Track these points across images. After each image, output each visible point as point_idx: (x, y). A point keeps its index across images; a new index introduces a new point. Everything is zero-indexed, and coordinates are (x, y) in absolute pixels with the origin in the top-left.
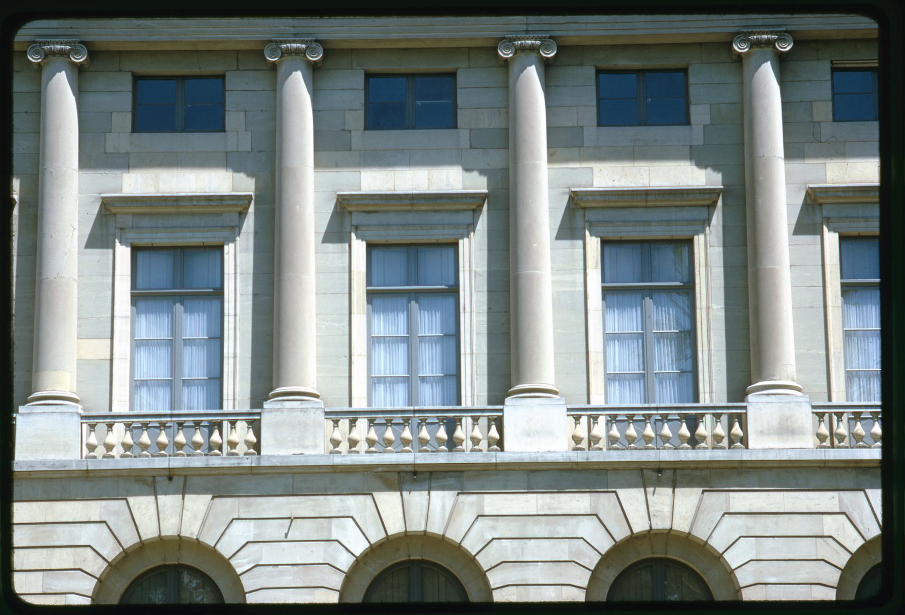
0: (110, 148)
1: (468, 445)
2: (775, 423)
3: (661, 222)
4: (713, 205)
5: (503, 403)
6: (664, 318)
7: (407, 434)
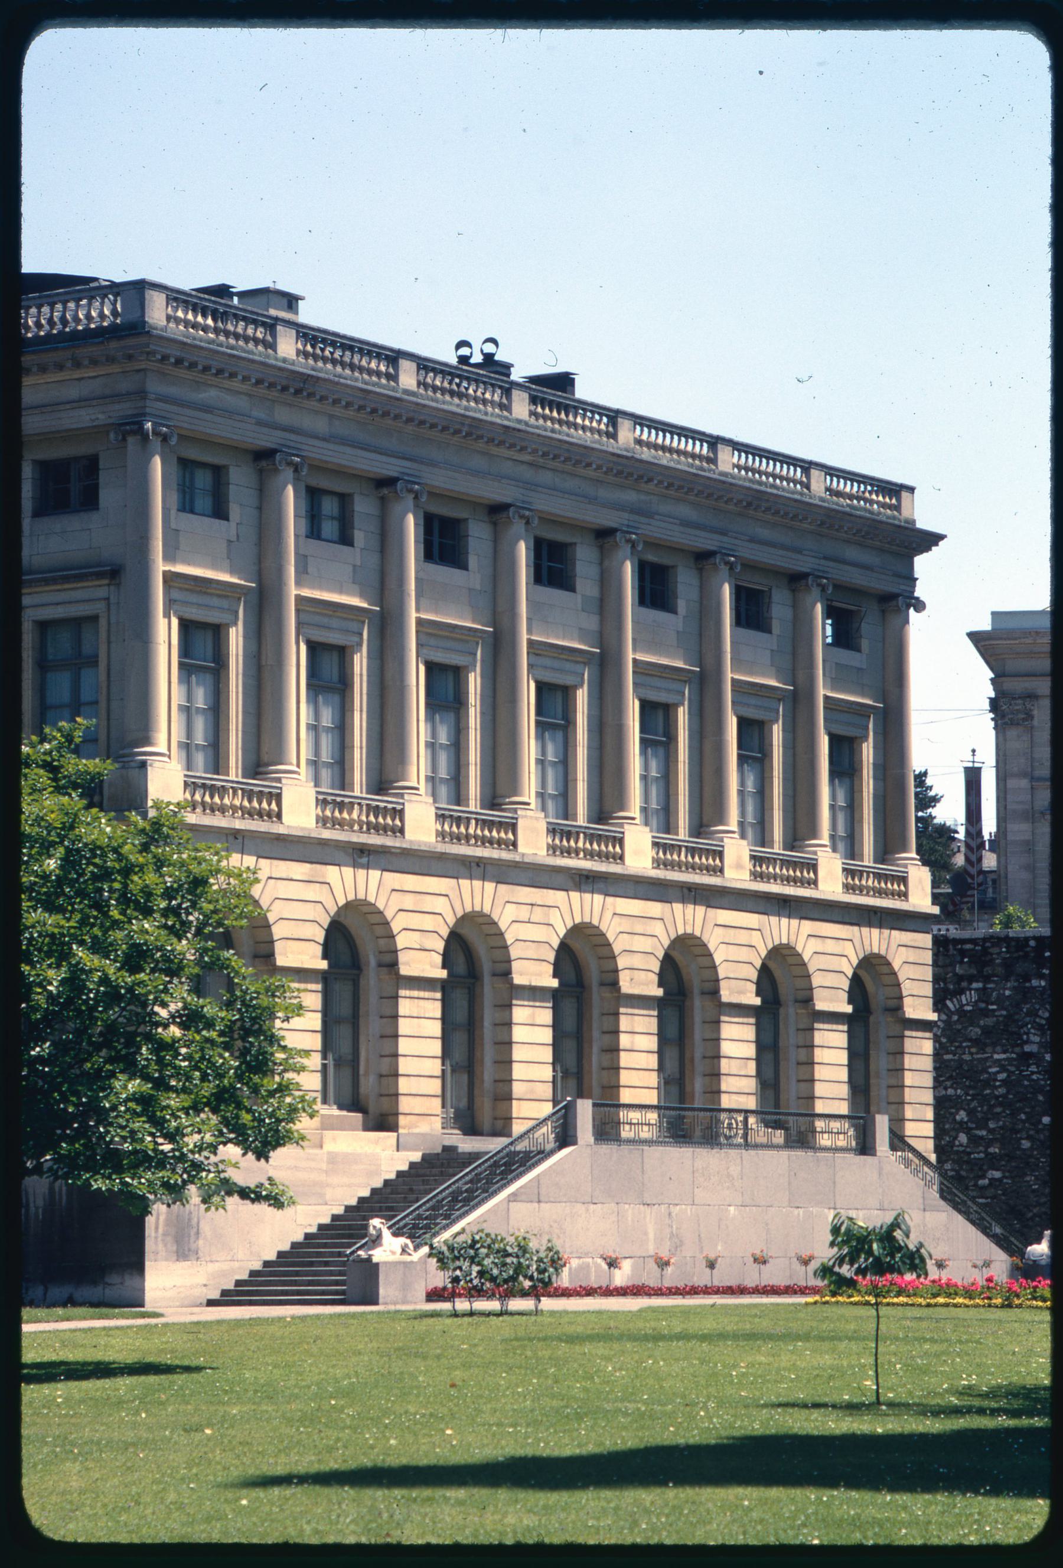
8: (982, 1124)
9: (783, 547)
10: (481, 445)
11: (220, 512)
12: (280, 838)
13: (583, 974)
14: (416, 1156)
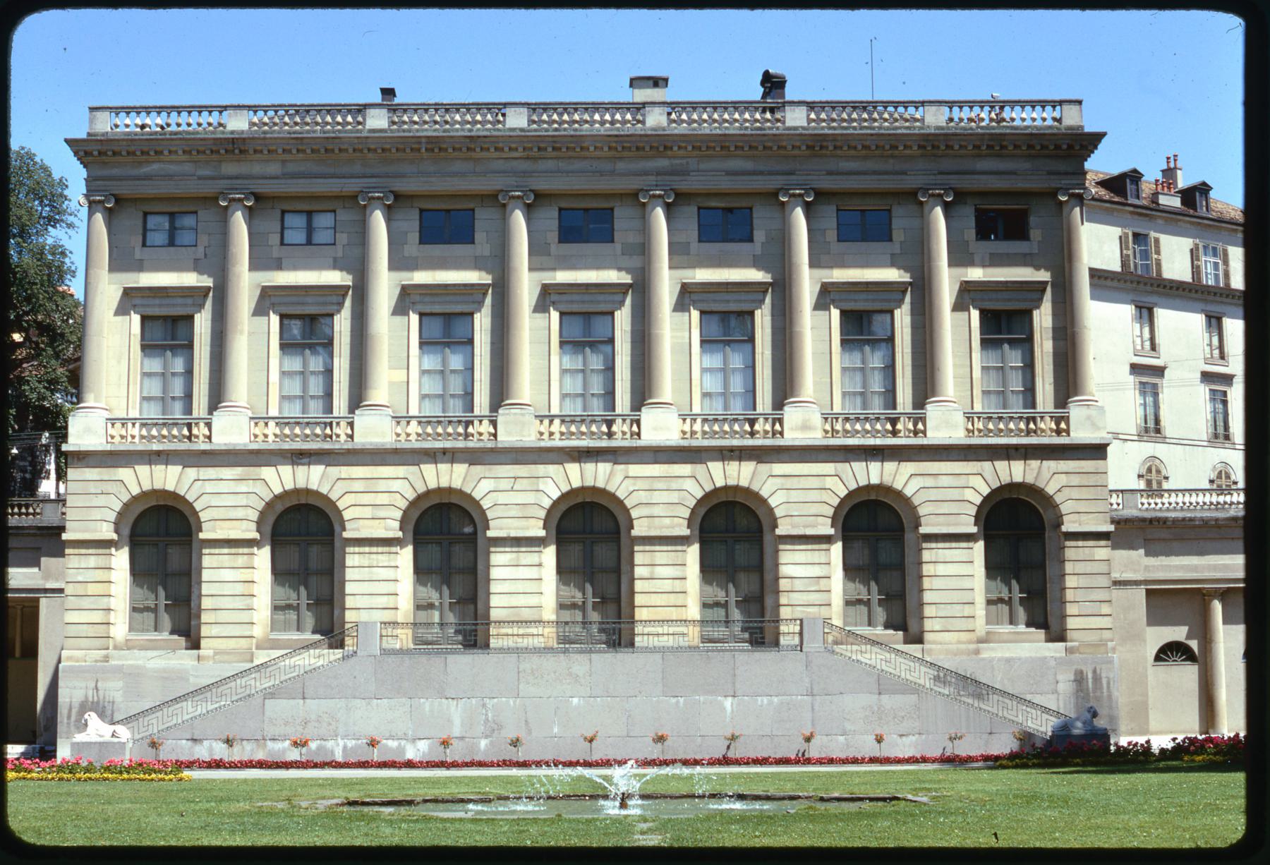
0: (406, 254)
1: (619, 435)
2: (800, 423)
3: (736, 301)
4: (766, 291)
5: (640, 410)
6: (1014, 358)
7: (584, 429)
9: (875, 173)
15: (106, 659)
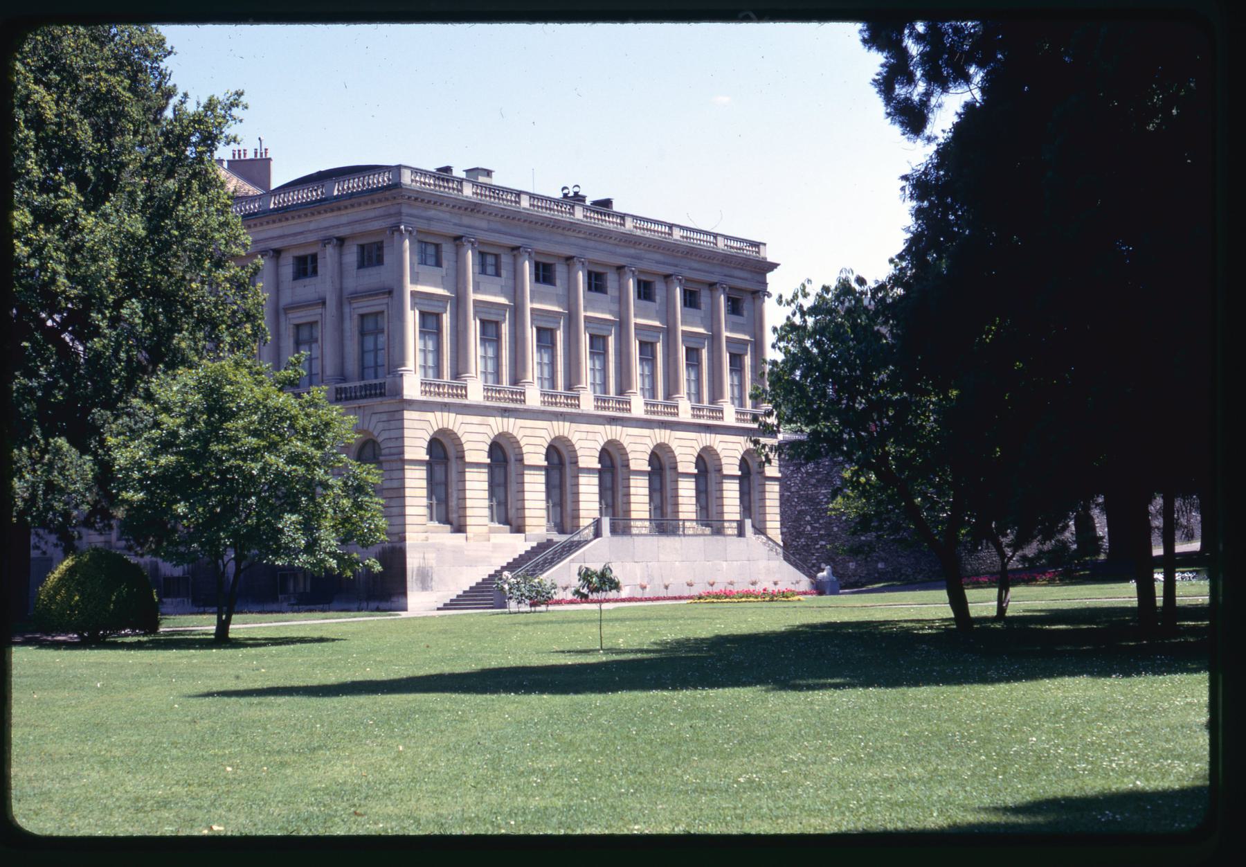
8: (817, 521)
10: (560, 230)
11: (438, 264)
12: (466, 406)
13: (612, 463)
14: (534, 544)
15: (427, 539)
